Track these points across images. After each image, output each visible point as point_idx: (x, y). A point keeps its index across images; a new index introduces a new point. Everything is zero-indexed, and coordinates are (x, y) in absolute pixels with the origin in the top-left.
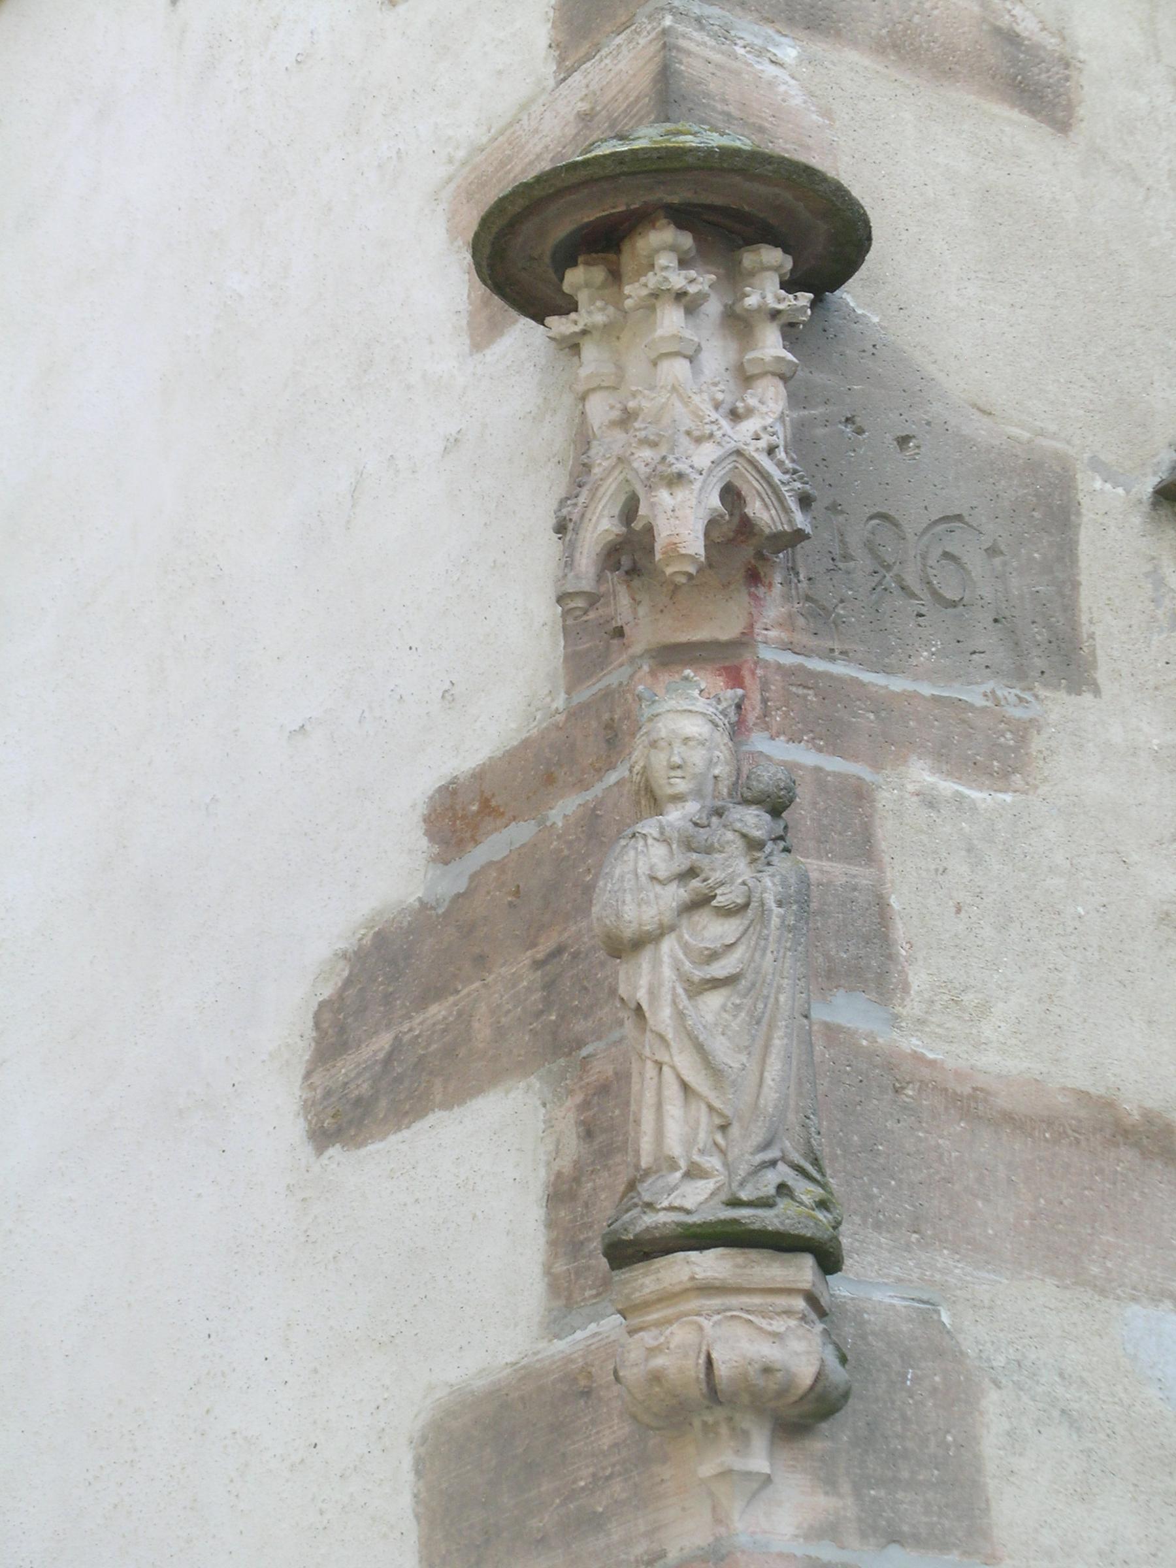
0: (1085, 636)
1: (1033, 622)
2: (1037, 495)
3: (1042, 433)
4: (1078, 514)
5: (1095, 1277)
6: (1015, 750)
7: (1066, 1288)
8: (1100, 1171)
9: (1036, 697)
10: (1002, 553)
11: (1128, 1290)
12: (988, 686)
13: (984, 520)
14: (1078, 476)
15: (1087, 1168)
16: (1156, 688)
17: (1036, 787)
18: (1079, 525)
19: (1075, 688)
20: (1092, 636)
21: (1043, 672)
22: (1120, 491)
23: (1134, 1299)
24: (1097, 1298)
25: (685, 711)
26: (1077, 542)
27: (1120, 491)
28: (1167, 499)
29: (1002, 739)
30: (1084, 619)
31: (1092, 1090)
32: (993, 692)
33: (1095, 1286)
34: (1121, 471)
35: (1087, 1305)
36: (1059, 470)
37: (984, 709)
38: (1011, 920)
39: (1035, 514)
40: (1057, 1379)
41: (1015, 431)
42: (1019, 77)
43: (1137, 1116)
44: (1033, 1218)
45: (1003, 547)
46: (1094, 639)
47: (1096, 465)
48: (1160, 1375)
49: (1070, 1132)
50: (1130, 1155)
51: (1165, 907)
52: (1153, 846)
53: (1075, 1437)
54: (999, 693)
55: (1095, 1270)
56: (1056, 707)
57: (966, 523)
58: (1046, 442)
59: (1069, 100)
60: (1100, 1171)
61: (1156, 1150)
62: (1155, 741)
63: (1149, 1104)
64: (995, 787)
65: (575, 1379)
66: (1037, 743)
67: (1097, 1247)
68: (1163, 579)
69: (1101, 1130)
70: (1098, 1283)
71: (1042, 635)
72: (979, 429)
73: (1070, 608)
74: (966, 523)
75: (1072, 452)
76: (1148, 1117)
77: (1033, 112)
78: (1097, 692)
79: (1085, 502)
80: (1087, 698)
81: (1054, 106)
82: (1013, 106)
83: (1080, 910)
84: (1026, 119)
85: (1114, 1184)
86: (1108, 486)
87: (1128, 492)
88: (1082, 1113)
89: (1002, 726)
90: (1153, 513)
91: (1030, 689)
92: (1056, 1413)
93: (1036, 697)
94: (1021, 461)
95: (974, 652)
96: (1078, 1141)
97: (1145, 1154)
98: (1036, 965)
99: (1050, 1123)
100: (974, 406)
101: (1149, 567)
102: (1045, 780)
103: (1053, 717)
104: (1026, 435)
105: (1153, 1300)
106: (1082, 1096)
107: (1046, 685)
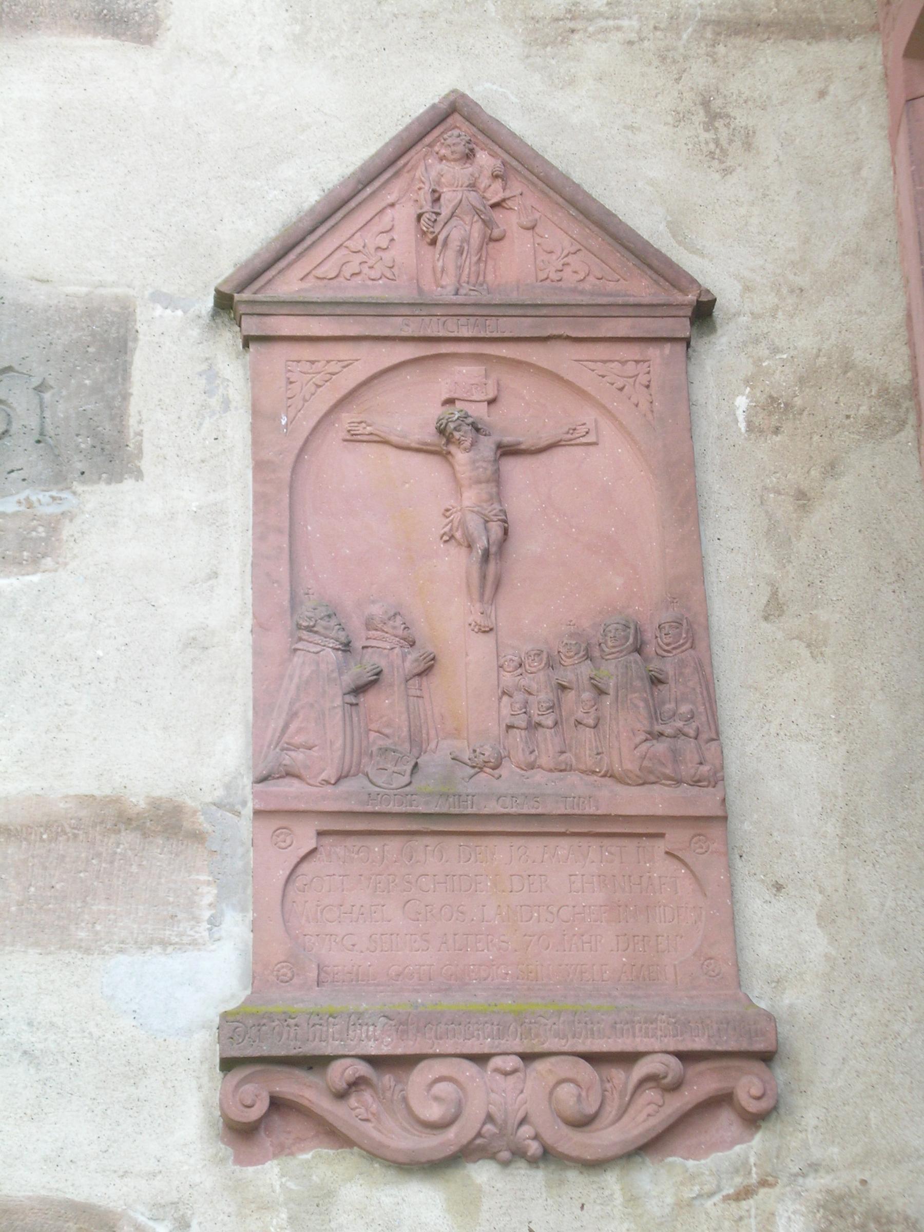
0: (132, 434)
1: (77, 435)
2: (93, 334)
3: (102, 285)
4: (136, 340)
5: (81, 940)
6: (47, 539)
7: (50, 953)
8: (99, 855)
9: (74, 493)
10: (52, 387)
11: (116, 945)
12: (22, 496)
13: (35, 365)
14: (138, 311)
15: (83, 855)
16: (203, 461)
17: (66, 564)
18: (135, 349)
19: (116, 477)
20: (140, 434)
21: (83, 473)
22: (179, 313)
23: (121, 951)
24: (80, 956)
25: (294, 470)
26: (131, 363)
27: (179, 313)
28: (223, 309)
29: (34, 534)
30: (132, 421)
31: (96, 793)
32: (28, 498)
33: (81, 947)
34: (183, 296)
35: (68, 964)
36: (118, 310)
37: (15, 514)
38: (24, 673)
39: (90, 350)
40: (25, 1027)
41: (71, 289)
42: (105, 12)
43: (143, 805)
44: (20, 904)
45: (52, 383)
46: (142, 436)
47: (158, 297)
48: (135, 1007)
49: (68, 830)
50: (128, 838)
51: (192, 634)
52: (185, 587)
53: (32, 1071)
54: (34, 498)
55: (82, 934)
56: (94, 497)
57: (17, 372)
58: (103, 291)
59: (157, 16)
60: (99, 855)
61: (159, 828)
62: (194, 504)
63: (157, 793)
64: (23, 572)
65: (417, 1007)
66: (67, 530)
67: (86, 917)
68: (218, 373)
69: (102, 822)
70: (83, 944)
71: (85, 443)
72: (40, 295)
73: (119, 416)
74: (17, 372)
75: (131, 292)
76: (155, 804)
77: (116, 35)
78: (138, 475)
79: (142, 328)
80: (129, 484)
81: (140, 25)
82: (96, 34)
83: (100, 653)
84: (110, 42)
85: (112, 862)
86: (169, 311)
87: (185, 312)
88: (83, 813)
89: (35, 522)
90: (212, 324)
91: (67, 488)
92: (16, 1056)
93: (74, 493)
94: (79, 311)
95: (13, 471)
96: (75, 836)
97: (145, 834)
98: (46, 705)
99: (47, 827)
100: (34, 279)
101: (204, 366)
102: (75, 556)
103: (89, 506)
104: (84, 290)
105: (141, 948)
106: (86, 800)
107: (84, 483)
